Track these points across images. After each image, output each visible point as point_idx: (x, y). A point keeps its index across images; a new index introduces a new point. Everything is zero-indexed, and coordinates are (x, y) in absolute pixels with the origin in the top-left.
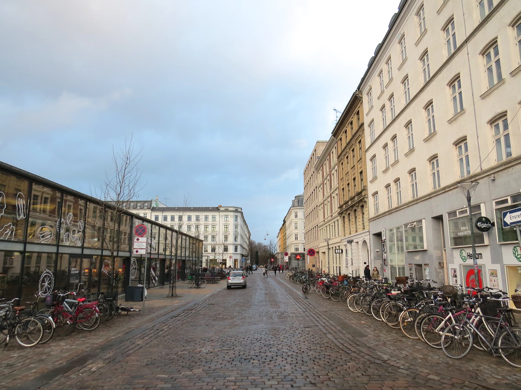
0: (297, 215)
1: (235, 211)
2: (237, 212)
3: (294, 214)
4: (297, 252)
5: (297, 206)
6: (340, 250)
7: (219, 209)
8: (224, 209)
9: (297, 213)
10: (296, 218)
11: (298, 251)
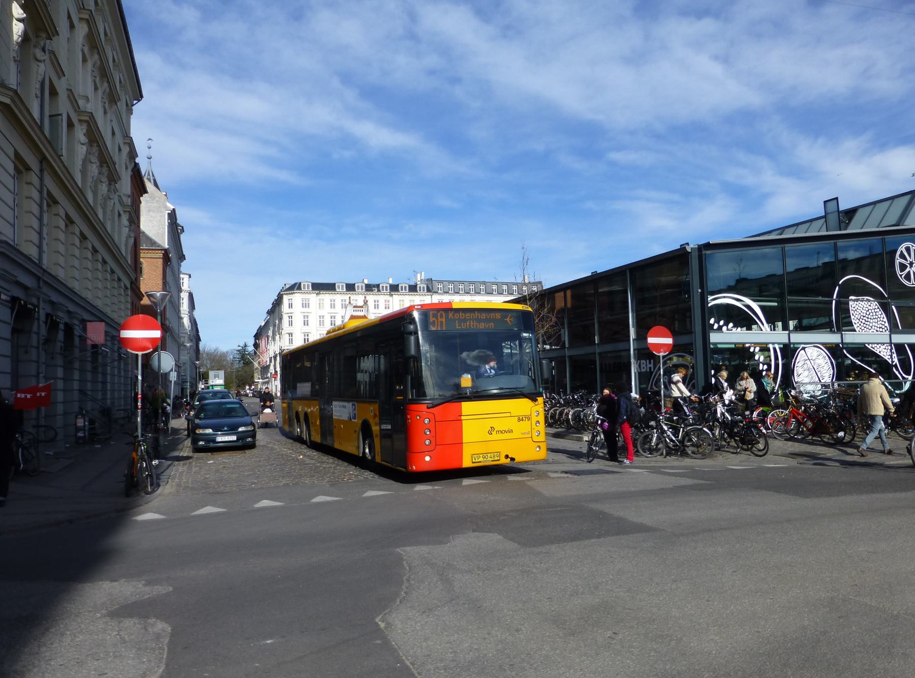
3: (374, 303)
10: (376, 309)
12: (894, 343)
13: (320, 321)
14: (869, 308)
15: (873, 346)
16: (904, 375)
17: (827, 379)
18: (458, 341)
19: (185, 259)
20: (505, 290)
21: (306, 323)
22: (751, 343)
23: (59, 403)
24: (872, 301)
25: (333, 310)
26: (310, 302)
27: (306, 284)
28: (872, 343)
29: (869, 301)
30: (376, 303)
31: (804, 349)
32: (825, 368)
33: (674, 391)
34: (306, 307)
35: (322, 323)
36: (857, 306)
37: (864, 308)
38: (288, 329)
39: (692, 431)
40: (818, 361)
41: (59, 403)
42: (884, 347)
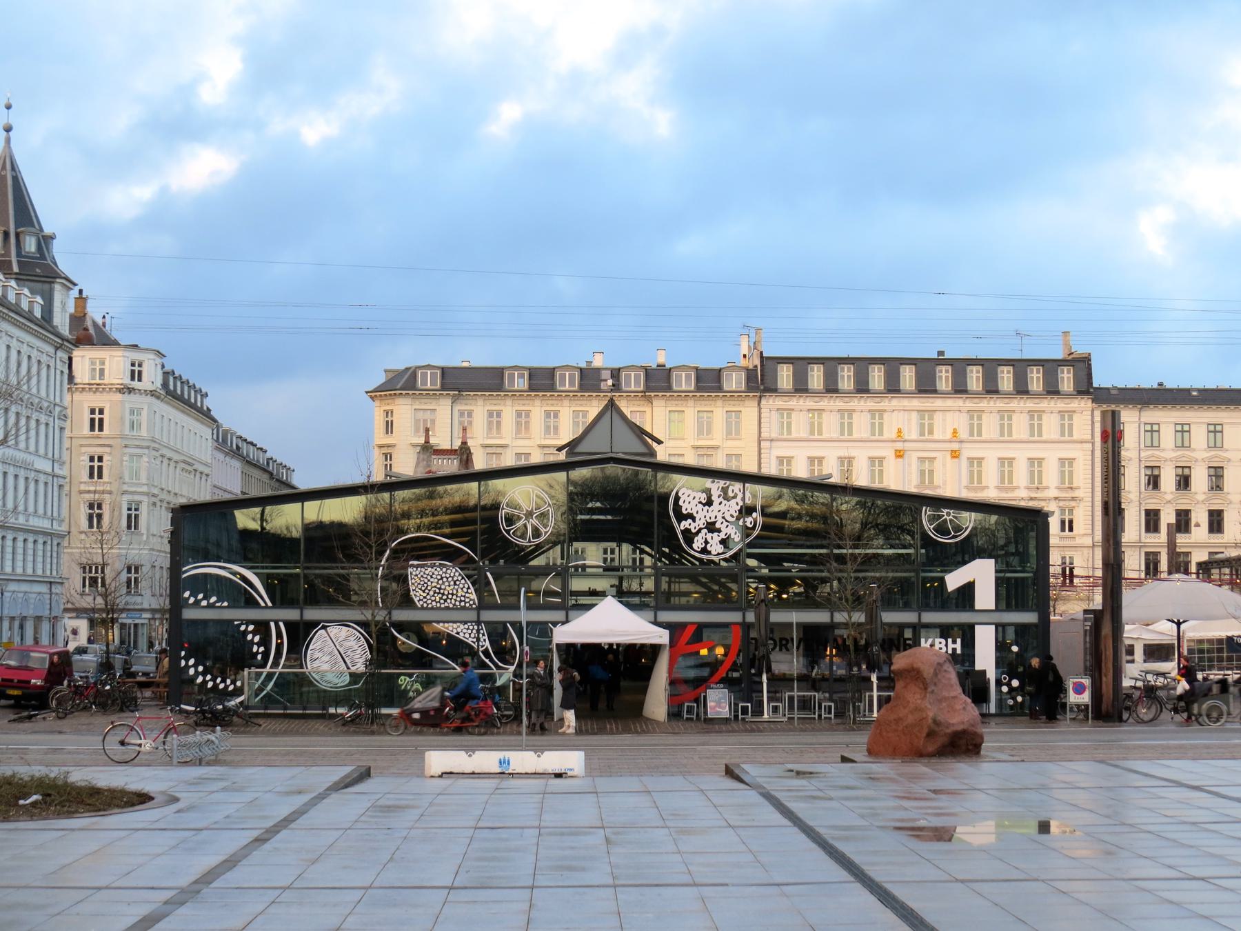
12: (485, 623)
14: (444, 575)
15: (446, 625)
16: (500, 664)
17: (360, 667)
18: (478, 514)
22: (242, 620)
24: (450, 566)
28: (444, 622)
29: (445, 566)
30: (96, 464)
31: (324, 628)
32: (358, 652)
33: (691, 667)
36: (422, 573)
37: (434, 576)
40: (346, 644)
42: (466, 626)
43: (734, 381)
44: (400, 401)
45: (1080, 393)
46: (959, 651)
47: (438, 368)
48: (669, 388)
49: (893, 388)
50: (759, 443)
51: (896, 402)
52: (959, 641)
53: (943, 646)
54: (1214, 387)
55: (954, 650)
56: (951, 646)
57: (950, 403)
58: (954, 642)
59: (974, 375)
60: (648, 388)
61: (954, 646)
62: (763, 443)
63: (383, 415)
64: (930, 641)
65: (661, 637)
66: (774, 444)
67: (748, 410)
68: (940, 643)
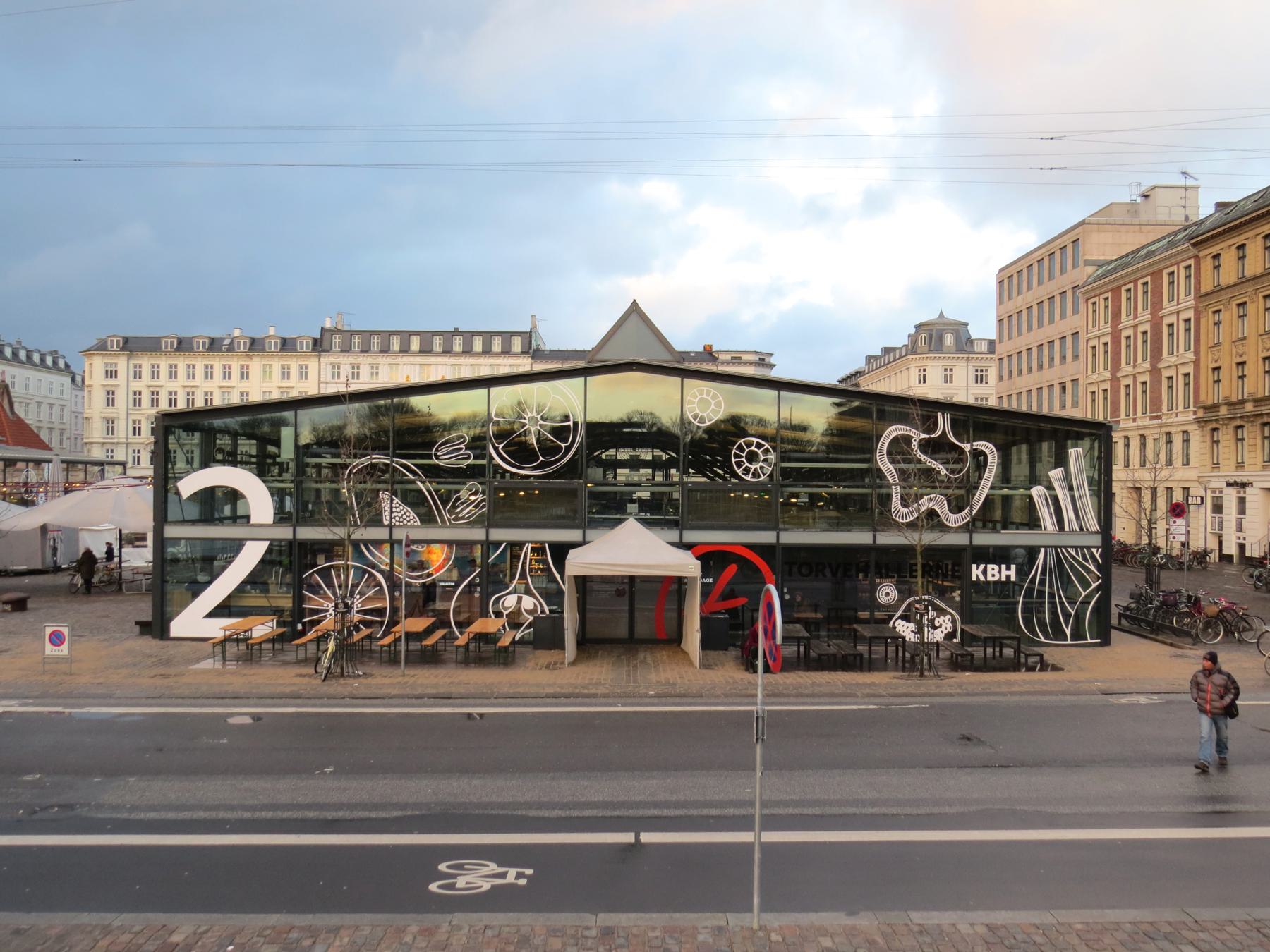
0: (924, 376)
1: (759, 364)
2: (763, 365)
3: (918, 373)
4: (173, 408)
5: (927, 350)
6: (1199, 499)
7: (717, 359)
8: (728, 357)
9: (924, 370)
10: (922, 384)
11: (175, 406)
13: (135, 399)
19: (966, 325)
20: (378, 343)
21: (110, 402)
23: (874, 536)
25: (226, 383)
26: (250, 370)
27: (169, 341)
34: (111, 377)
35: (154, 402)
38: (105, 410)
39: (717, 697)
41: (874, 536)
43: (306, 345)
44: (95, 358)
45: (523, 353)
46: (1013, 579)
47: (120, 337)
48: (263, 350)
49: (405, 350)
50: (319, 384)
51: (406, 359)
52: (1013, 567)
53: (996, 572)
54: (582, 349)
55: (1008, 577)
56: (1004, 572)
57: (439, 359)
58: (1008, 569)
59: (438, 342)
60: (251, 349)
61: (1008, 573)
62: (321, 385)
63: (150, 367)
64: (982, 566)
65: (688, 565)
66: (329, 385)
67: (313, 364)
68: (993, 569)
